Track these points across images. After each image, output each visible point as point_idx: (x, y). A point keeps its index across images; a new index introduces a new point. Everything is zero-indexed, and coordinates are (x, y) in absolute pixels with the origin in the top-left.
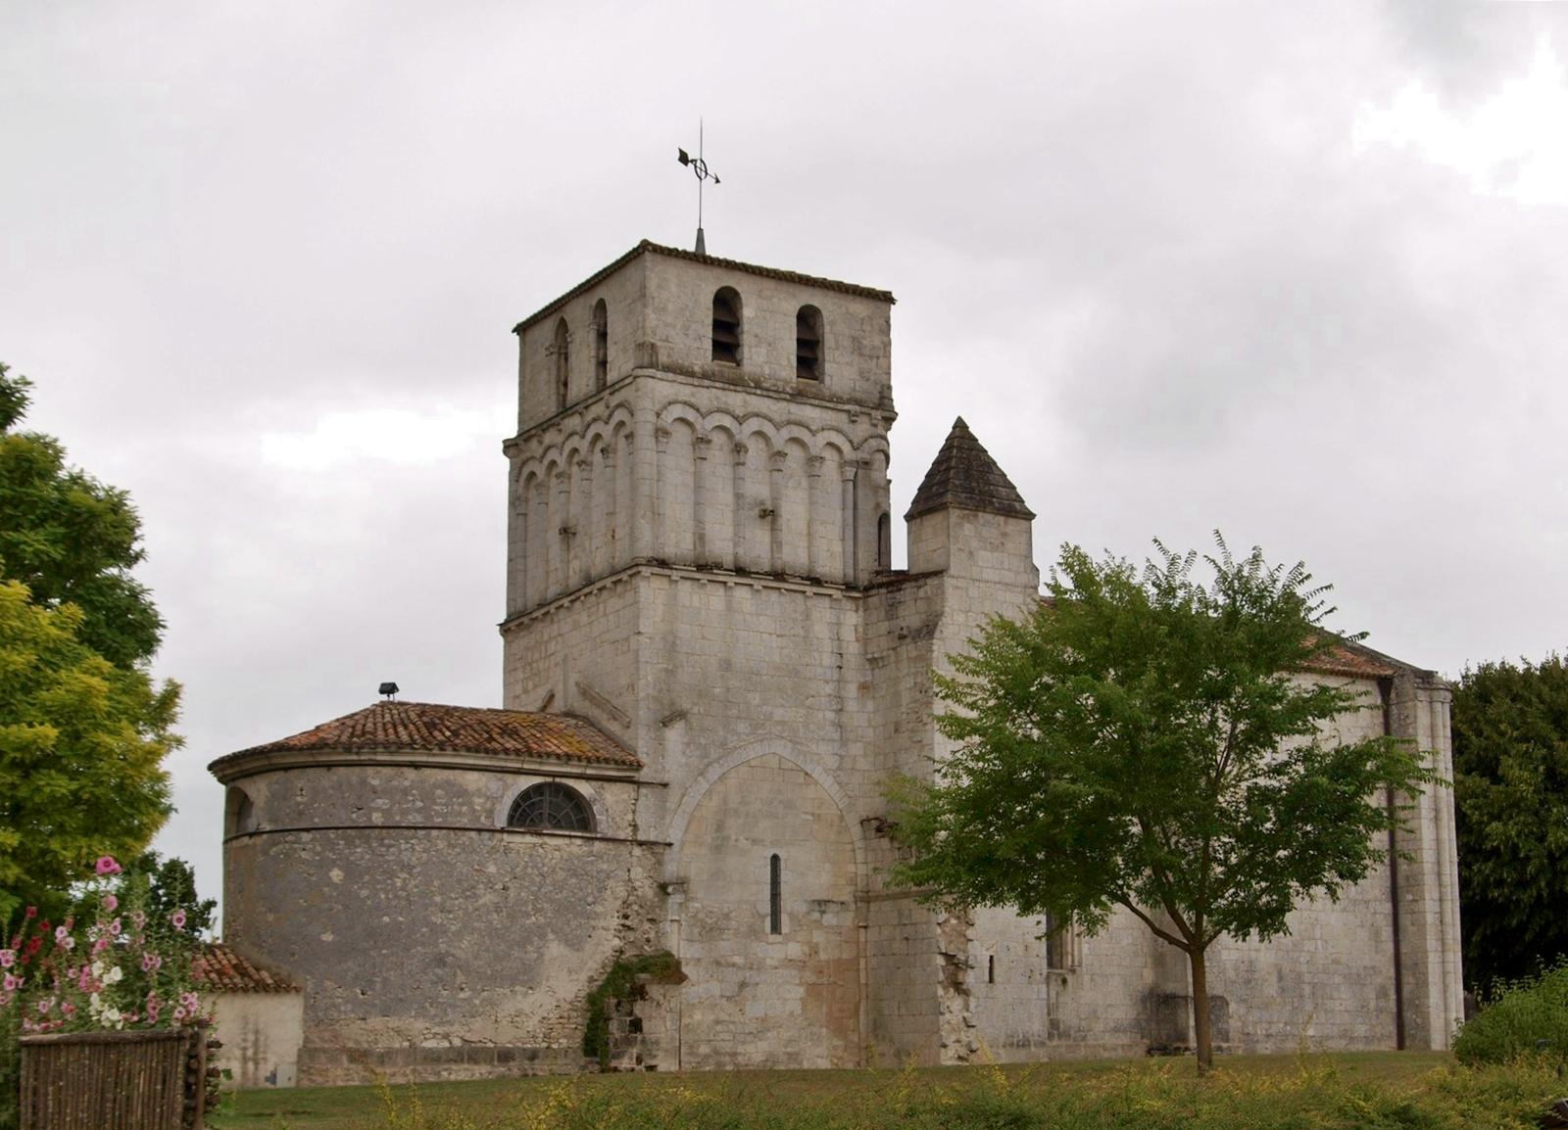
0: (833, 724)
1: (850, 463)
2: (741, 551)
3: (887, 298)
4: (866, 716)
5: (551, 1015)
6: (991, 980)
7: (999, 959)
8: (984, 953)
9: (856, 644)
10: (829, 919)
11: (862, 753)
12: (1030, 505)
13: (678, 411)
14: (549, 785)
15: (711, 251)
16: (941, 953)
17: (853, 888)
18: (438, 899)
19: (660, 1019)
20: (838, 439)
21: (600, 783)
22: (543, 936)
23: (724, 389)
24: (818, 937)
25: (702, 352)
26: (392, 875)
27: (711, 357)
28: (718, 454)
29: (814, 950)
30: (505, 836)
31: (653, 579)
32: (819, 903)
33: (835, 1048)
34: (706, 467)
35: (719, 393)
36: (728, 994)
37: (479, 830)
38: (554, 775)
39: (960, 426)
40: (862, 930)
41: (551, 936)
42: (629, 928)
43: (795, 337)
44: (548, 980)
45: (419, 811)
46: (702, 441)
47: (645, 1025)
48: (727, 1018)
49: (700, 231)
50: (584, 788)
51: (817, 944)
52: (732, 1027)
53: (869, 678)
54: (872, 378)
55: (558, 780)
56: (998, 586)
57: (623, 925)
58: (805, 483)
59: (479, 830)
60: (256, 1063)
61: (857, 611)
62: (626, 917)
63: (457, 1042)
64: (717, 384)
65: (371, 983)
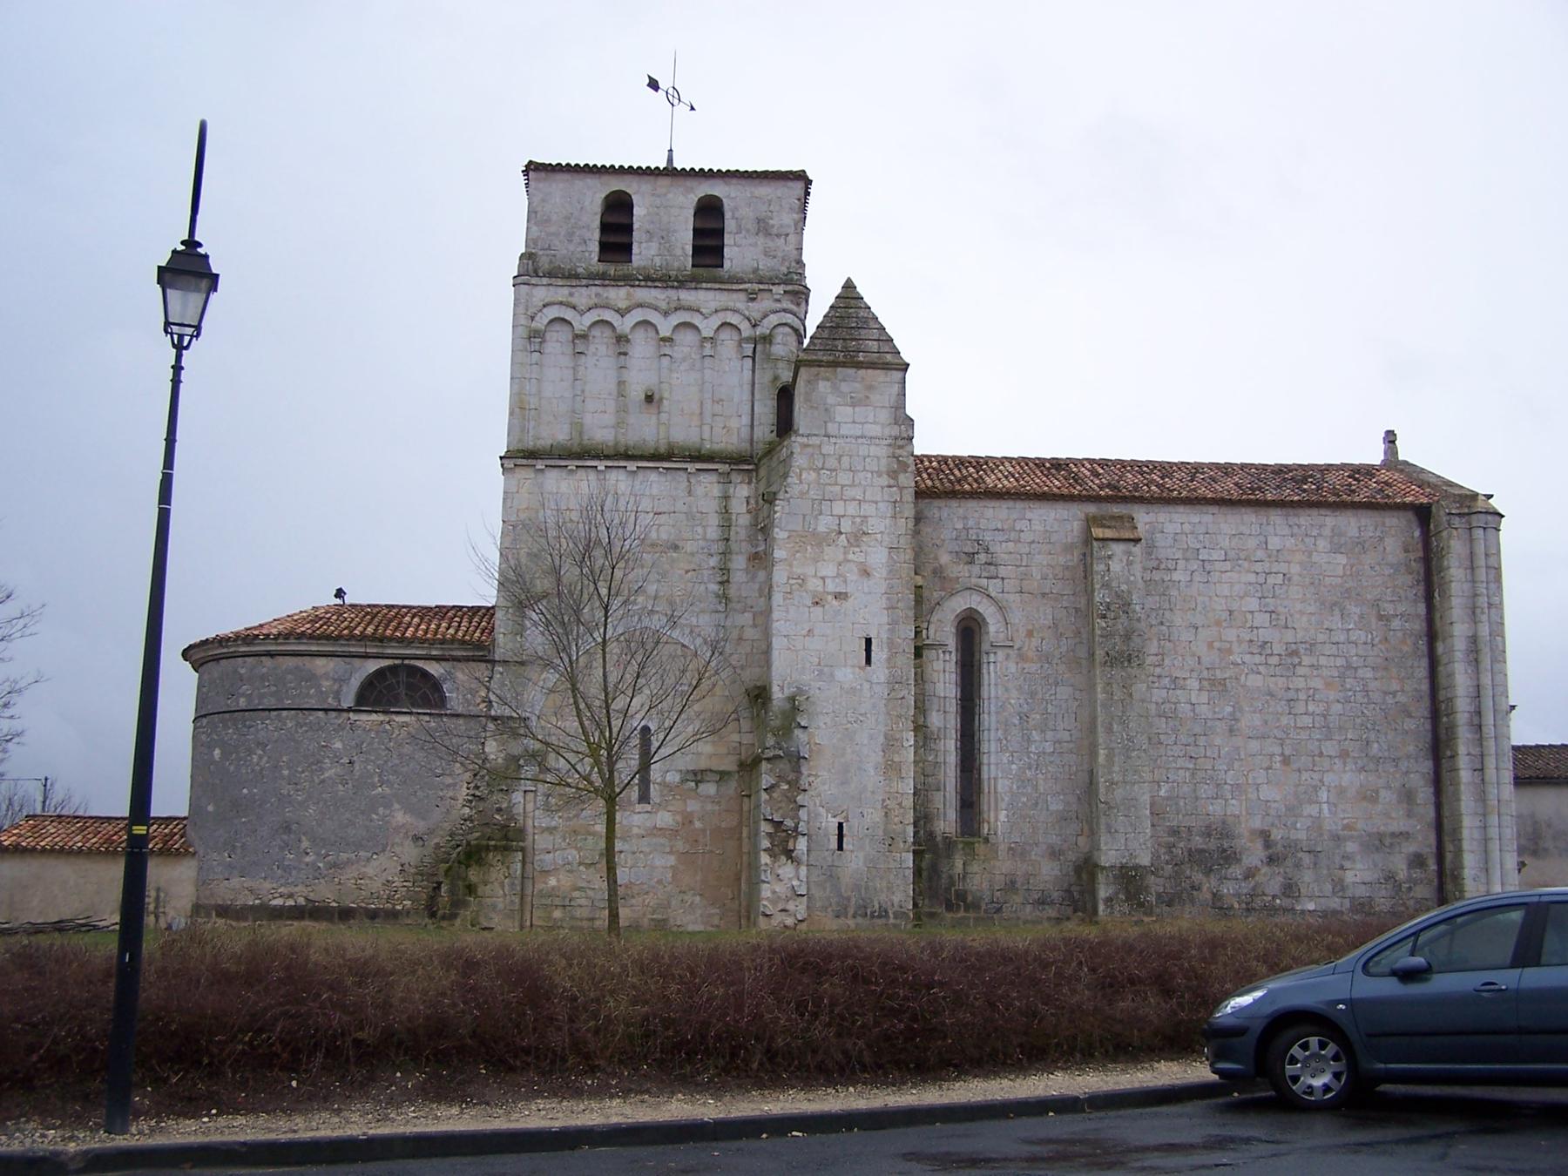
1: (748, 340)
3: (801, 178)
4: (757, 586)
6: (840, 848)
7: (850, 828)
10: (709, 789)
13: (553, 312)
18: (286, 772)
19: (497, 886)
20: (734, 319)
22: (388, 806)
24: (693, 806)
26: (250, 752)
28: (601, 345)
29: (688, 820)
30: (351, 715)
32: (695, 773)
33: (711, 916)
34: (588, 361)
35: (599, 290)
37: (326, 710)
39: (849, 286)
41: (396, 806)
42: (480, 798)
45: (273, 694)
46: (621, 339)
50: (434, 669)
51: (692, 813)
52: (591, 893)
54: (780, 254)
58: (566, 361)
59: (326, 710)
60: (157, 918)
61: (749, 483)
63: (301, 901)
65: (234, 847)
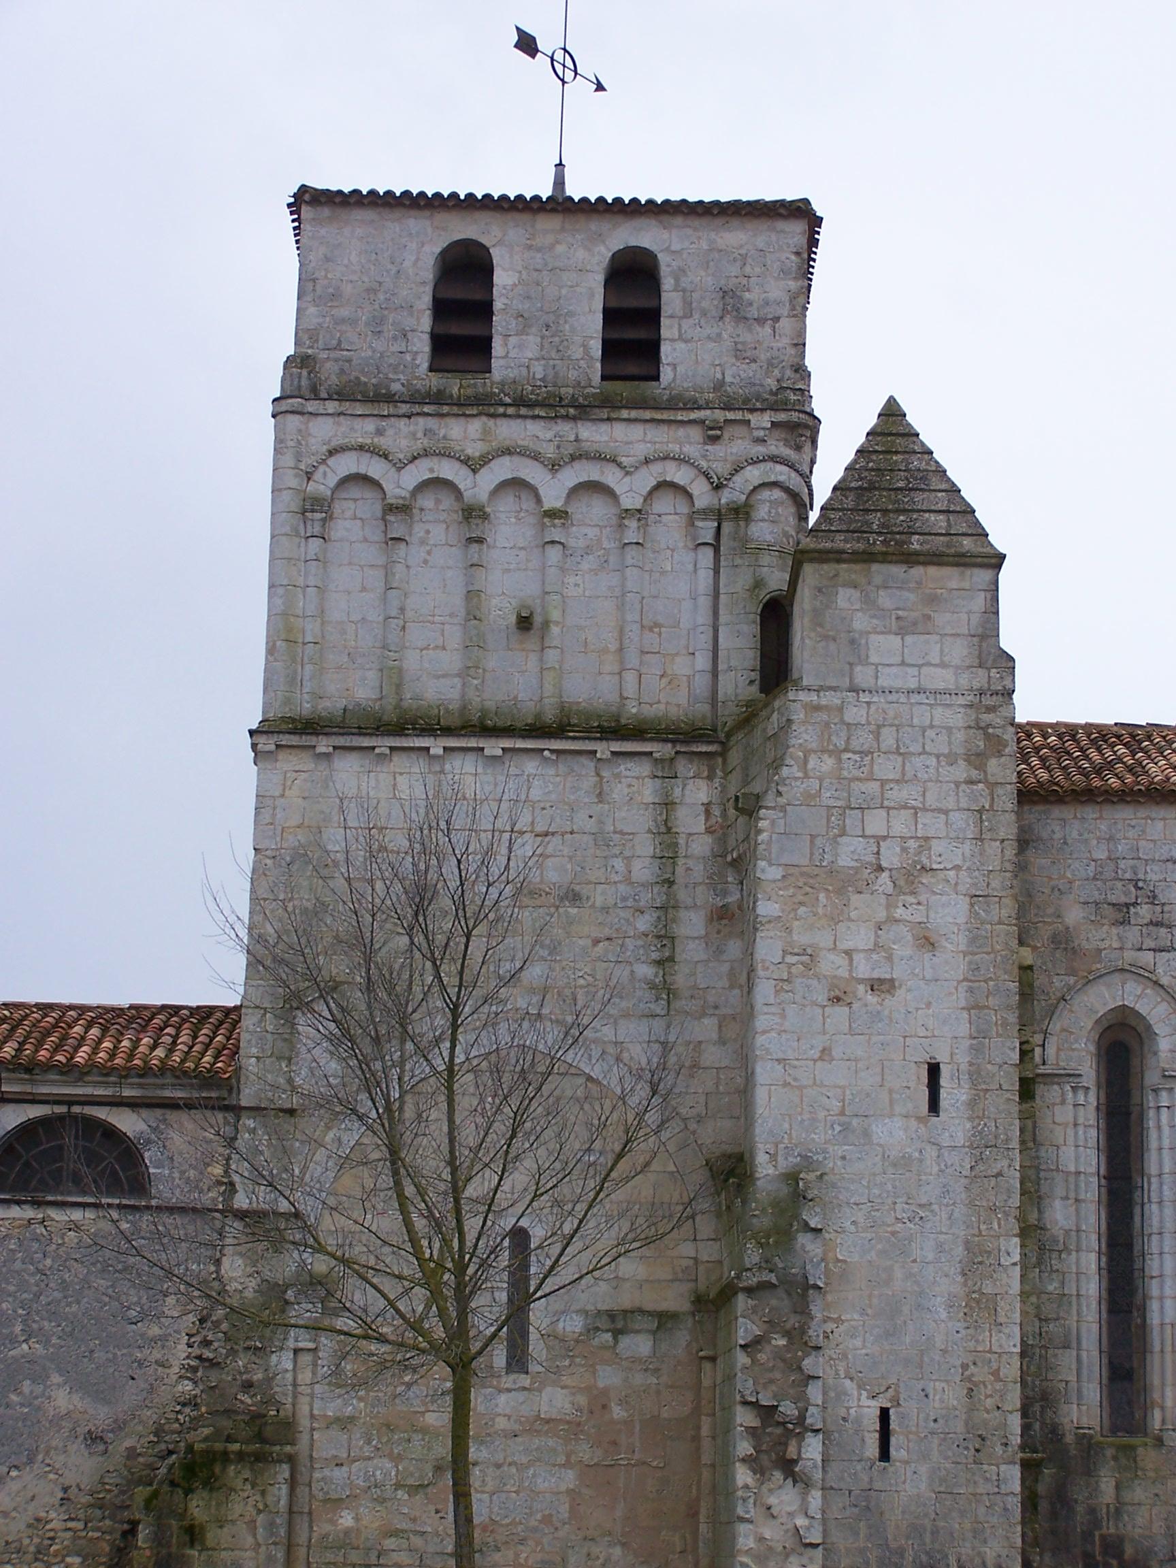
0: (653, 986)
1: (705, 513)
2: (471, 693)
3: (801, 214)
4: (725, 968)
5: (53, 1515)
8: (865, 1401)
9: (708, 839)
11: (715, 1036)
12: (998, 540)
13: (347, 464)
14: (61, 1118)
15: (575, 190)
16: (745, 1403)
17: (691, 1285)
20: (680, 475)
21: (158, 1112)
23: (442, 415)
24: (608, 1377)
25: (408, 357)
27: (426, 365)
28: (435, 528)
29: (599, 1402)
31: (282, 755)
32: (611, 1315)
35: (432, 423)
36: (410, 1481)
38: (70, 1102)
39: (892, 412)
40: (707, 1366)
41: (56, 1379)
42: (213, 1364)
43: (599, 305)
44: (47, 1453)
46: (472, 514)
47: (212, 1536)
48: (405, 1525)
49: (560, 165)
50: (128, 1123)
51: (605, 1392)
52: (417, 1541)
53: (733, 898)
55: (76, 1109)
56: (915, 698)
57: (199, 1358)
61: (710, 778)
62: (206, 1343)
64: (426, 409)
